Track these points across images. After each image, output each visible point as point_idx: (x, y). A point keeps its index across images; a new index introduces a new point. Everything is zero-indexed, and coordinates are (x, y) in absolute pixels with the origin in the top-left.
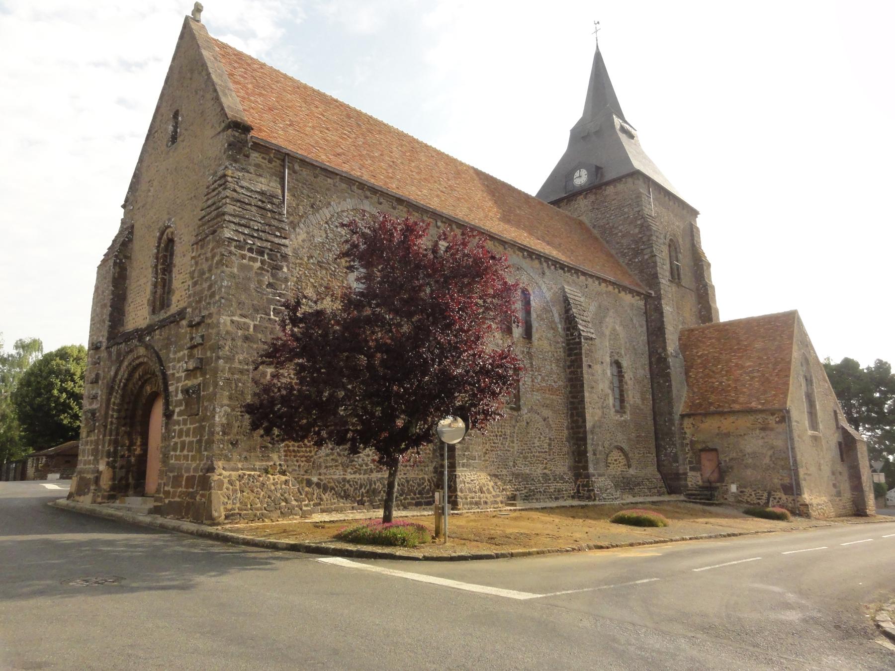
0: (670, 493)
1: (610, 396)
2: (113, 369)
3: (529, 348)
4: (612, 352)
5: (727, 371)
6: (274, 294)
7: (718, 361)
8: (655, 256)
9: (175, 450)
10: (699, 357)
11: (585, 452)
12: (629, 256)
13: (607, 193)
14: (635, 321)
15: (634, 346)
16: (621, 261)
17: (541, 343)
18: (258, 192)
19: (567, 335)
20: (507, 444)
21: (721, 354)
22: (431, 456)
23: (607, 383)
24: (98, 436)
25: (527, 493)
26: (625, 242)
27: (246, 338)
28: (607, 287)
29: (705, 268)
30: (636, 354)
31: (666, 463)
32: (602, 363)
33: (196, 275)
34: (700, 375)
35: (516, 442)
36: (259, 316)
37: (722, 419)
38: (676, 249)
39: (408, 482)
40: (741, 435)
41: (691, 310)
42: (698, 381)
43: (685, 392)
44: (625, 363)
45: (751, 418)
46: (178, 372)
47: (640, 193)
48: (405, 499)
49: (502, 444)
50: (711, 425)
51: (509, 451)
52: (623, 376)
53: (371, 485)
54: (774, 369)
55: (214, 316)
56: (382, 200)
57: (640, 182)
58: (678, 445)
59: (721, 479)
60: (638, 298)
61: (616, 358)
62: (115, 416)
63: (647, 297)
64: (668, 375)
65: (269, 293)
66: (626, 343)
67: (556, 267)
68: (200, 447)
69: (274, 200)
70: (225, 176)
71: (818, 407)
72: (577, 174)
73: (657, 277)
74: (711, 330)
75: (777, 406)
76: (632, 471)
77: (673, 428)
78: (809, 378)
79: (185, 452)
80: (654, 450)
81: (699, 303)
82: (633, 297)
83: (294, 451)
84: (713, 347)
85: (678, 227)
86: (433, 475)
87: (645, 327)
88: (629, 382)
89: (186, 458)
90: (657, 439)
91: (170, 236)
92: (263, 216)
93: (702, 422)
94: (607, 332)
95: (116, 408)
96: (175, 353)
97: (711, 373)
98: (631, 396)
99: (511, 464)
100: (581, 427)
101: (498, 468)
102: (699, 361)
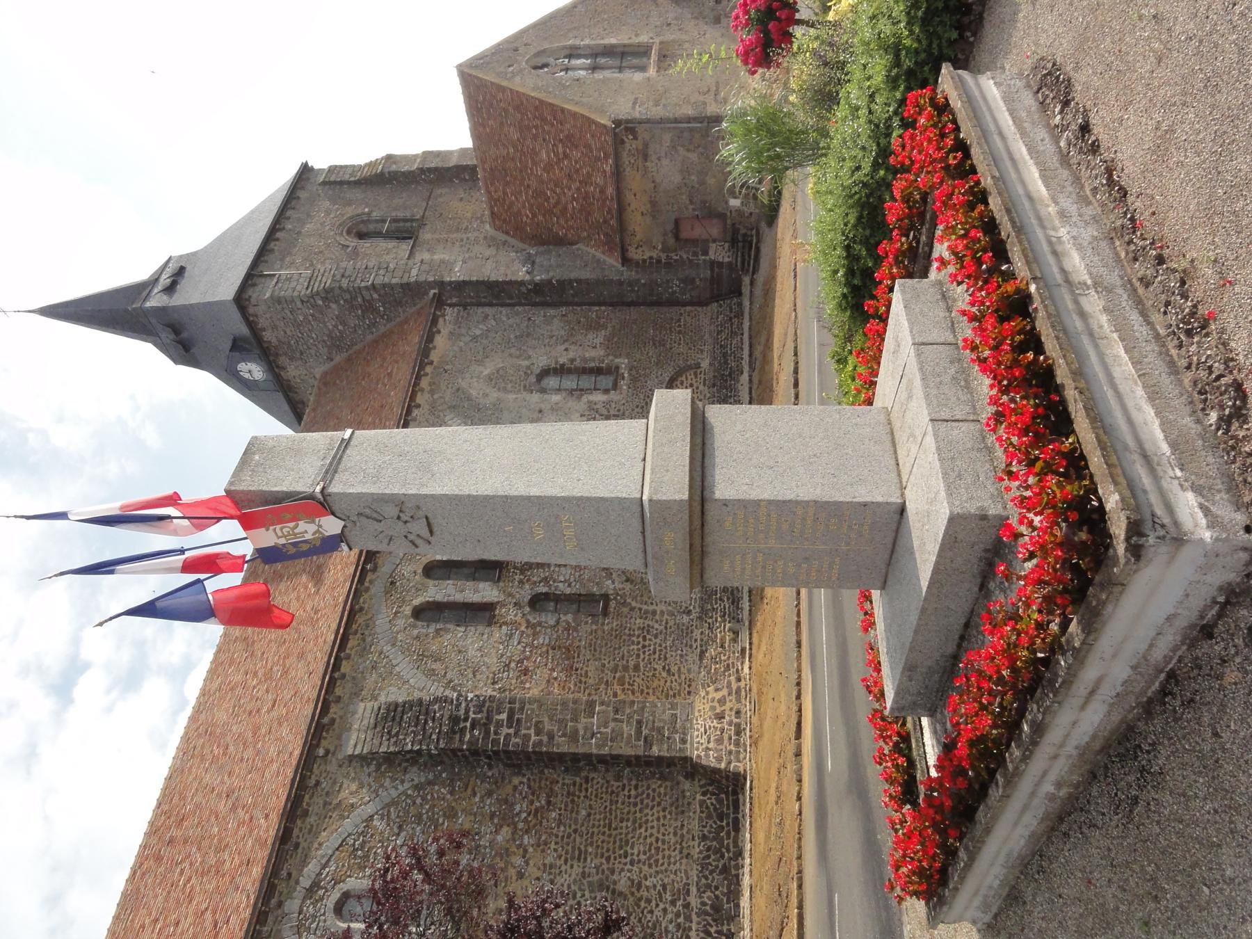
0: (740, 294)
3: (515, 568)
5: (556, 185)
7: (539, 194)
8: (373, 284)
10: (534, 215)
12: (375, 318)
13: (274, 340)
14: (478, 332)
15: (516, 337)
16: (382, 329)
20: (656, 626)
21: (528, 186)
22: (668, 784)
25: (728, 599)
26: (352, 322)
28: (422, 390)
29: (394, 168)
30: (528, 335)
31: (694, 293)
32: (540, 411)
34: (562, 222)
35: (654, 607)
37: (629, 210)
38: (363, 222)
39: (704, 838)
40: (655, 187)
41: (461, 199)
42: (572, 227)
43: (589, 249)
45: (628, 172)
47: (272, 297)
48: (728, 851)
50: (638, 223)
53: (707, 914)
54: (553, 125)
56: (284, 873)
57: (253, 293)
59: (722, 217)
60: (441, 320)
61: (533, 379)
63: (440, 302)
64: (561, 283)
66: (511, 355)
71: (613, 41)
73: (408, 284)
74: (492, 189)
75: (609, 139)
76: (705, 364)
77: (643, 281)
78: (567, 52)
80: (673, 311)
81: (451, 181)
82: (439, 332)
84: (520, 192)
85: (328, 213)
86: (696, 782)
87: (487, 310)
88: (571, 355)
90: (658, 303)
93: (634, 235)
94: (494, 395)
97: (560, 207)
99: (686, 619)
101: (691, 646)
102: (540, 218)
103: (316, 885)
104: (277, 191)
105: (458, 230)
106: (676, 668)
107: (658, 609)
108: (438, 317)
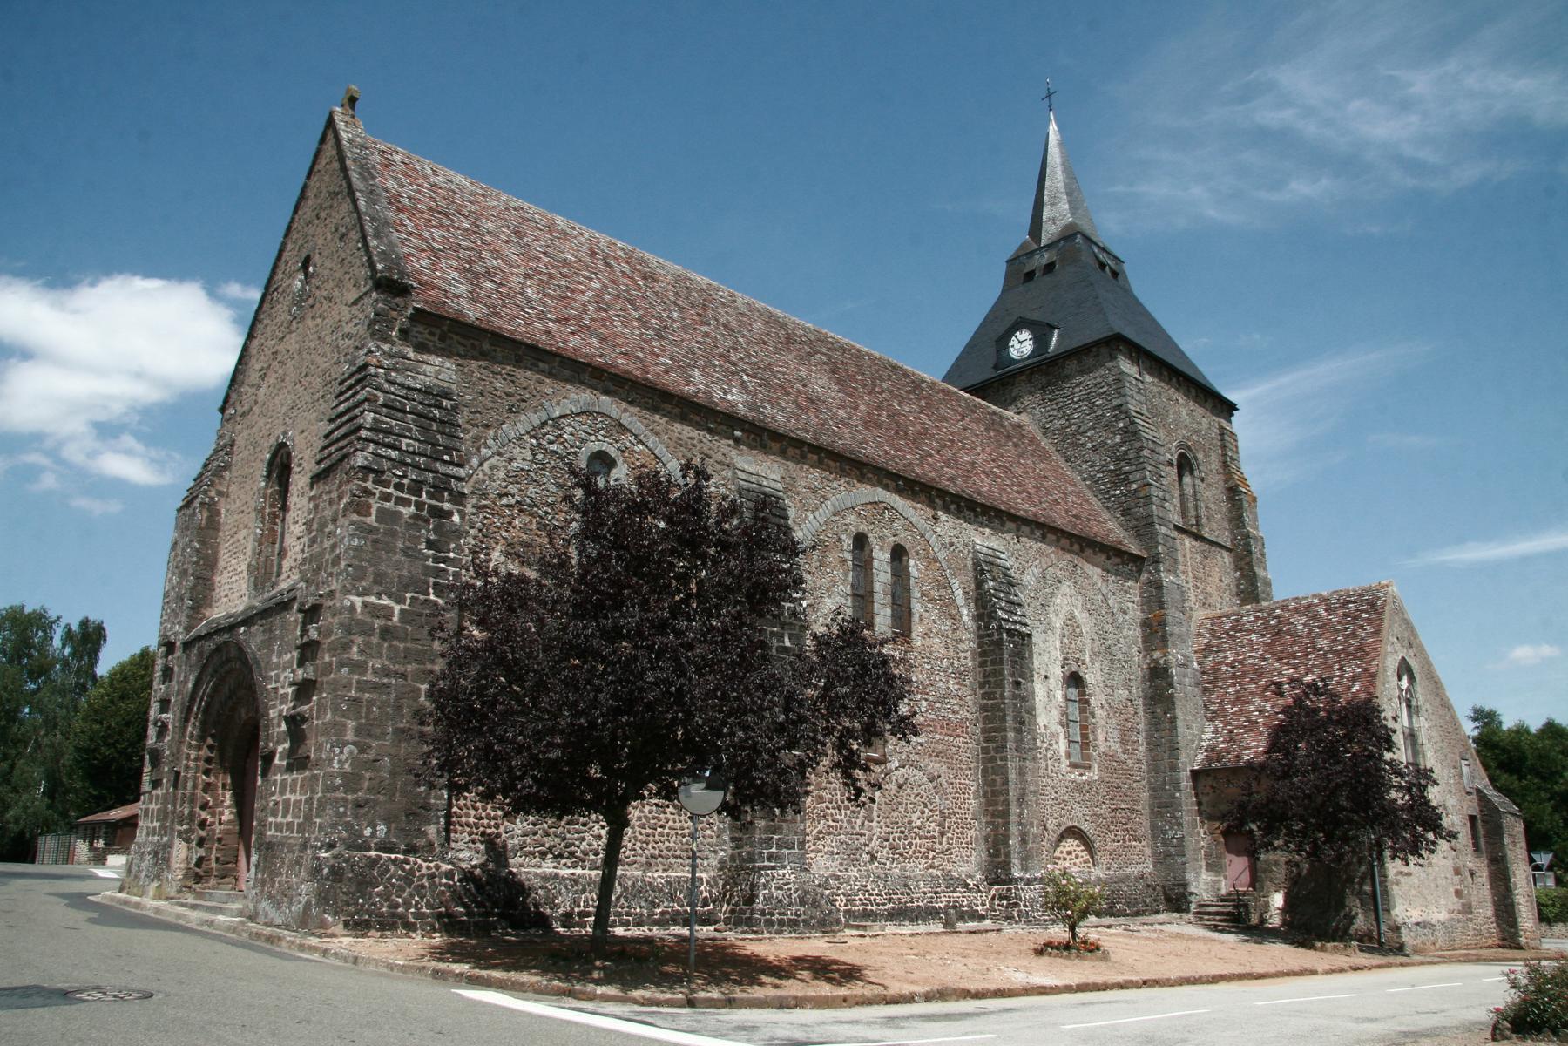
1: (1062, 736)
2: (192, 678)
4: (1066, 659)
6: (437, 560)
9: (275, 815)
11: (1007, 837)
14: (1111, 602)
17: (928, 642)
18: (419, 390)
19: (979, 628)
20: (859, 822)
23: (1056, 715)
24: (167, 790)
27: (386, 633)
32: (1046, 677)
33: (315, 526)
35: (876, 819)
36: (408, 595)
44: (1092, 677)
46: (283, 687)
47: (1122, 373)
49: (849, 822)
51: (862, 835)
52: (1087, 702)
55: (338, 595)
58: (1185, 825)
60: (1118, 560)
62: (192, 757)
65: (428, 557)
67: (959, 506)
68: (311, 810)
69: (445, 403)
70: (365, 366)
72: (1014, 342)
79: (289, 819)
82: (1109, 558)
83: (468, 825)
88: (1098, 712)
89: (290, 826)
91: (285, 461)
92: (424, 429)
94: (1058, 623)
95: (193, 742)
96: (280, 655)
98: (1101, 737)
100: (1000, 793)
103: (623, 429)
104: (1201, 373)
105: (1195, 577)
106: (821, 847)
107: (874, 824)
108: (1121, 557)
